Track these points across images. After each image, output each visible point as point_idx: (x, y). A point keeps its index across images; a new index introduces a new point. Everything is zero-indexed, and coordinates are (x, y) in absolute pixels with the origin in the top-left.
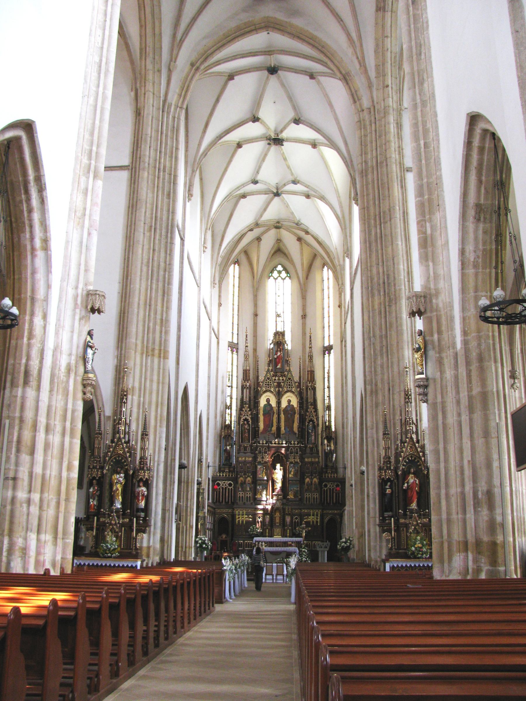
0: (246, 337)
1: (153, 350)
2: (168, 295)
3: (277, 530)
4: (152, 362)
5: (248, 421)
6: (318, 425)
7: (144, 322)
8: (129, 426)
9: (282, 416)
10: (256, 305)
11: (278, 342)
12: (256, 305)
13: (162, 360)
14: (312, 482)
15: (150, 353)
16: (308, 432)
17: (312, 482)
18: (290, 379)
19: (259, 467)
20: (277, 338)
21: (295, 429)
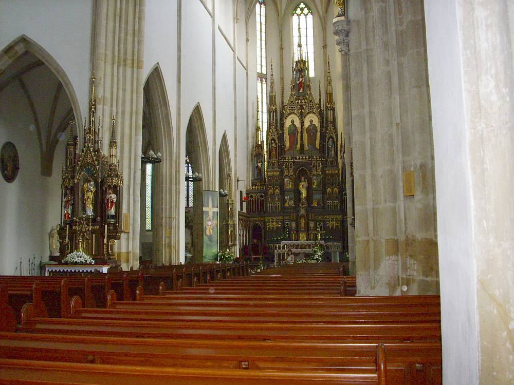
0: (271, 67)
1: (125, 60)
2: (140, 5)
3: (303, 235)
4: (125, 71)
5: (275, 141)
6: (337, 141)
7: (114, 33)
8: (98, 135)
9: (306, 135)
10: (281, 40)
11: (299, 70)
12: (281, 40)
13: (135, 70)
14: (332, 192)
15: (122, 63)
16: (328, 147)
17: (332, 192)
18: (311, 101)
19: (286, 180)
20: (299, 66)
21: (318, 146)
